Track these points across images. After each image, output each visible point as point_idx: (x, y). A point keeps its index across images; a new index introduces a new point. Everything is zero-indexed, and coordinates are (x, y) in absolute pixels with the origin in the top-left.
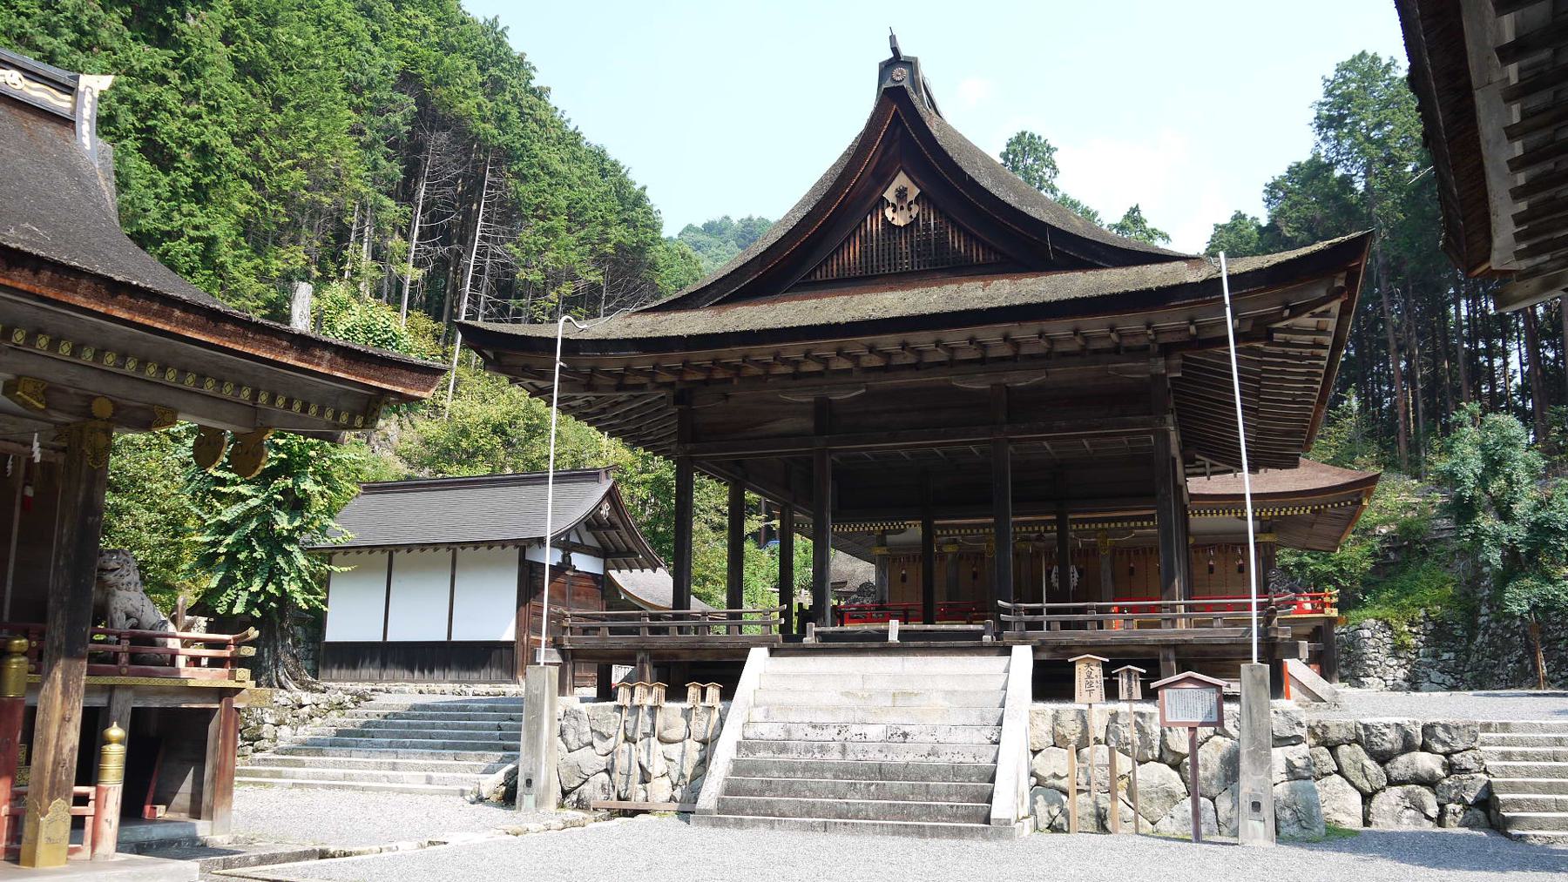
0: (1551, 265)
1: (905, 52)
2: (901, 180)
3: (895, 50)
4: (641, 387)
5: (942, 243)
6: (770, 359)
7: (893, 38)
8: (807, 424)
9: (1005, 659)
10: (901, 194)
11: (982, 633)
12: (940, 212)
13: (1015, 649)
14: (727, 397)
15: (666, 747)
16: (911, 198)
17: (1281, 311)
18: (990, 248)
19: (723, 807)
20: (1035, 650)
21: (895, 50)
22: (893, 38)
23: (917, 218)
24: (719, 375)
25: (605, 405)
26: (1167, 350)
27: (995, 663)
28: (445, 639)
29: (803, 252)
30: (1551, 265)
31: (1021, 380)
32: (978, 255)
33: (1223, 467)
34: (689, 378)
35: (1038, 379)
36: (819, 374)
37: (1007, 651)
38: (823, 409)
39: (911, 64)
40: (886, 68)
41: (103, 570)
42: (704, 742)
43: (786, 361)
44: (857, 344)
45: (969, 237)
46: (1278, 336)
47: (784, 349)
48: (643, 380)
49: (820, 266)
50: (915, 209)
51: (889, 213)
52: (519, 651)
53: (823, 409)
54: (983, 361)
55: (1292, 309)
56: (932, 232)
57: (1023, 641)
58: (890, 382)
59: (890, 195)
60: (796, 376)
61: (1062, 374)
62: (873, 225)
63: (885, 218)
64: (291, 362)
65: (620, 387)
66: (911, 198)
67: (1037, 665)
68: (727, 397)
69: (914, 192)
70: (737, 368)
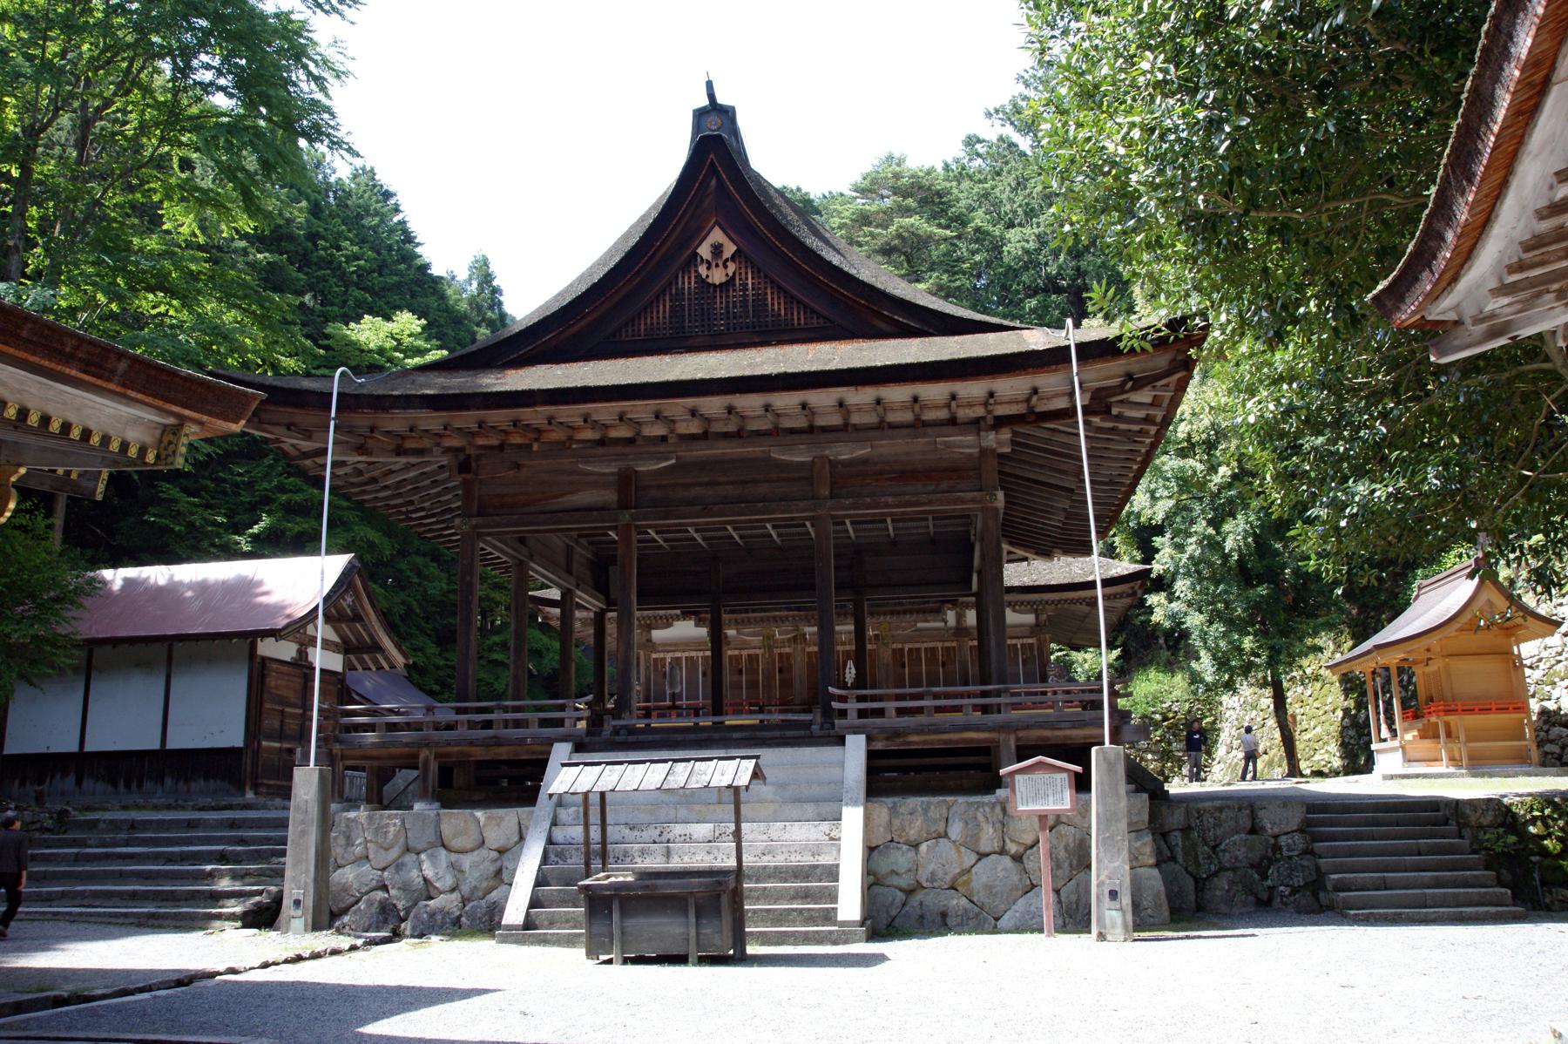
0: (1508, 310)
1: (720, 100)
2: (717, 236)
3: (711, 96)
4: (420, 452)
5: (760, 303)
6: (579, 422)
7: (709, 85)
8: (610, 496)
9: (837, 749)
10: (717, 250)
11: (810, 723)
12: (757, 271)
13: (849, 738)
14: (518, 466)
15: (454, 857)
16: (727, 254)
17: (1124, 383)
18: (813, 311)
19: (529, 924)
20: (869, 739)
21: (711, 96)
22: (709, 85)
23: (733, 278)
24: (516, 440)
25: (375, 474)
26: (1000, 422)
27: (828, 753)
28: (156, 745)
29: (616, 306)
30: (1508, 310)
31: (845, 452)
32: (798, 318)
33: (1021, 553)
34: (480, 442)
35: (862, 452)
36: (630, 441)
37: (841, 741)
38: (626, 482)
39: (728, 114)
40: (699, 114)
41: (1189, 87)
42: (501, 852)
43: (595, 425)
44: (676, 407)
45: (790, 298)
46: (1115, 411)
47: (596, 410)
48: (427, 443)
49: (626, 325)
50: (732, 267)
51: (703, 270)
52: (248, 761)
53: (626, 482)
54: (811, 429)
55: (1136, 381)
56: (750, 292)
57: (856, 730)
58: (701, 452)
59: (704, 251)
60: (602, 442)
61: (887, 448)
62: (688, 284)
63: (698, 276)
64: (74, 373)
65: (399, 451)
66: (727, 254)
67: (872, 755)
68: (518, 466)
69: (729, 249)
70: (539, 431)
